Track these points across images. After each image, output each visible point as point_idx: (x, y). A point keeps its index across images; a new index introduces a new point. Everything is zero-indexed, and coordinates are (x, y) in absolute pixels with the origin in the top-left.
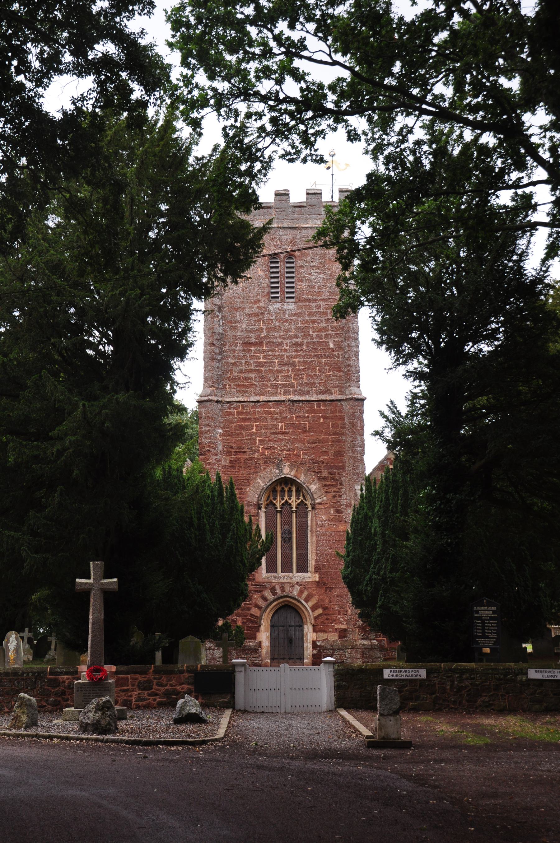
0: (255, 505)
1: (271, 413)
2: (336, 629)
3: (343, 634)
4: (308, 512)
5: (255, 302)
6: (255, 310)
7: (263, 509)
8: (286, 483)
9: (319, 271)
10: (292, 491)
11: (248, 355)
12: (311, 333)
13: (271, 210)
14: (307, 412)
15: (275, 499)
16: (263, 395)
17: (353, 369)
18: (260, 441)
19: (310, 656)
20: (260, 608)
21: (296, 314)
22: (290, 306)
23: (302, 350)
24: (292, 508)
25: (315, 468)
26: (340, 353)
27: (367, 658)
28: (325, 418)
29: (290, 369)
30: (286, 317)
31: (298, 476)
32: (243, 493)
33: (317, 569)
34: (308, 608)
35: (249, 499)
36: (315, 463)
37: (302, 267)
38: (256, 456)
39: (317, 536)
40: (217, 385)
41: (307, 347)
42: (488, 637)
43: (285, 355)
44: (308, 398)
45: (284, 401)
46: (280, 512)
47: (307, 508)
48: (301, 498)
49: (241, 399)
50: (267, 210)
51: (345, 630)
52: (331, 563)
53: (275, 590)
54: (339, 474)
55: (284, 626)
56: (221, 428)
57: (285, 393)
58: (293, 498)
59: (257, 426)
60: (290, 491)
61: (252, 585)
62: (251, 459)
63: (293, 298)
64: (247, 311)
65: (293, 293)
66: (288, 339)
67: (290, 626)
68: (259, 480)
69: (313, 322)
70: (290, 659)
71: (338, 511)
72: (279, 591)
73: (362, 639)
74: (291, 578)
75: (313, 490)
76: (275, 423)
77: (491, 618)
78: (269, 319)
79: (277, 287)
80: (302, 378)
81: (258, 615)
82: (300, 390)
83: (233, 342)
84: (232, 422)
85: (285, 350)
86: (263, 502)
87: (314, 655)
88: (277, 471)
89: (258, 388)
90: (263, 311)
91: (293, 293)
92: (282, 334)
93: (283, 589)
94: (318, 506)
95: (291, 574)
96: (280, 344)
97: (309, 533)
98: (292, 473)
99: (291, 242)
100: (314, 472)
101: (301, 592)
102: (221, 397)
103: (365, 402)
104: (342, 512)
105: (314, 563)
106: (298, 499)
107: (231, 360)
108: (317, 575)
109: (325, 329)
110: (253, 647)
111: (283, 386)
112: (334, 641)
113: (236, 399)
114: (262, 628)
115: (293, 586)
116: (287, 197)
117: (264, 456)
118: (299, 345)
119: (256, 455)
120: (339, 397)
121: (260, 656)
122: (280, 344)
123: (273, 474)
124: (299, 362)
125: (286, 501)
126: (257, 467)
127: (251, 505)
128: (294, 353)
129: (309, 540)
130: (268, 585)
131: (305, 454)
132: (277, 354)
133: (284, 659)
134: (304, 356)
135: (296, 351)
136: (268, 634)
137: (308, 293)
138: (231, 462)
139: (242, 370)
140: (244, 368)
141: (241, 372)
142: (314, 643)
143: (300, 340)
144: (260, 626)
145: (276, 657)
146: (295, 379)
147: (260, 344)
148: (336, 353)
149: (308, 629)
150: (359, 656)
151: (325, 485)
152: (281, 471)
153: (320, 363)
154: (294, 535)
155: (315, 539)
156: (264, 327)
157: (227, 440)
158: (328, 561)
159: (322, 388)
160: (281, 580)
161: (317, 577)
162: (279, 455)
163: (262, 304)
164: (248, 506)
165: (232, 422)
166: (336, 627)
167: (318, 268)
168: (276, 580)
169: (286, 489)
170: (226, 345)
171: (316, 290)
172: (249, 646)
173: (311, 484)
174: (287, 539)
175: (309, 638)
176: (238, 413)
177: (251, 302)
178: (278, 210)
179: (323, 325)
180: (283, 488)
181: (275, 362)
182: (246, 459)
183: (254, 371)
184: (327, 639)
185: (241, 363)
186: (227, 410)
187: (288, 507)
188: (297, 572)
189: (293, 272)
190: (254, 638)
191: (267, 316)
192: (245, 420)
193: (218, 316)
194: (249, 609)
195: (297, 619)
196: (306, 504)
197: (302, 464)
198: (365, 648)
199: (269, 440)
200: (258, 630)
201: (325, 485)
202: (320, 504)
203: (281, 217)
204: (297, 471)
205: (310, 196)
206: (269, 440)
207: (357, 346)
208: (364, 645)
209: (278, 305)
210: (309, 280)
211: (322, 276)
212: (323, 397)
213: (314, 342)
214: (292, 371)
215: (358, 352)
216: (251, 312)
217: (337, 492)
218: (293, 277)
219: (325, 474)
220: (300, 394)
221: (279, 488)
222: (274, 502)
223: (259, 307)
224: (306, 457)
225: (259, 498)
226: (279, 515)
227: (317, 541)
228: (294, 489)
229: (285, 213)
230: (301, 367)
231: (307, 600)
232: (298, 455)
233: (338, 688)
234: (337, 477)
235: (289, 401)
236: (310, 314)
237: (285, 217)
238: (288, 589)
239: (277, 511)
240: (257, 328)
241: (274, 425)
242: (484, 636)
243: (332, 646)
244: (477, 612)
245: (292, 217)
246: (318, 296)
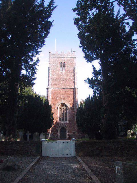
3: (74, 133)
6: (58, 72)
33: (69, 121)
42: (122, 131)
71: (73, 109)
77: (124, 125)
90: (59, 72)
114: (58, 132)
138: (53, 100)
142: (68, 135)
149: (67, 132)
150: (77, 137)
219: (71, 102)
231: (67, 126)
233: (76, 149)
242: (122, 131)
244: (119, 123)
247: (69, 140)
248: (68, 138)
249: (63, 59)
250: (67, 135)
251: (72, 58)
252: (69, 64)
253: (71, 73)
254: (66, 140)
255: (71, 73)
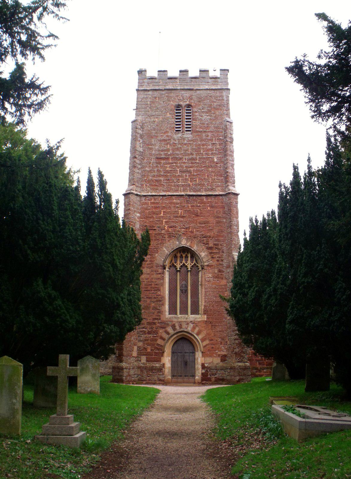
0: (161, 266)
1: (174, 203)
2: (219, 355)
4: (199, 271)
5: (165, 133)
6: (164, 137)
7: (167, 269)
8: (184, 251)
9: (208, 115)
10: (188, 257)
11: (159, 166)
12: (202, 152)
13: (177, 80)
14: (199, 203)
15: (176, 263)
16: (169, 191)
17: (230, 175)
18: (166, 222)
19: (200, 374)
20: (164, 339)
21: (191, 141)
22: (188, 135)
23: (196, 163)
24: (188, 269)
25: (204, 240)
26: (222, 165)
27: (241, 375)
28: (212, 207)
29: (187, 175)
30: (186, 142)
31: (192, 246)
32: (153, 258)
34: (199, 340)
35: (157, 262)
36: (204, 237)
37: (196, 112)
38: (163, 232)
39: (205, 289)
40: (137, 184)
41: (199, 160)
43: (184, 165)
44: (199, 193)
45: (183, 195)
46: (179, 271)
47: (199, 269)
48: (194, 262)
49: (154, 194)
50: (174, 80)
51: (225, 356)
52: (215, 307)
53: (175, 327)
54: (221, 245)
55: (181, 353)
56: (139, 213)
57: (184, 191)
58: (189, 262)
59: (164, 212)
60: (186, 257)
61: (159, 323)
62: (160, 234)
63: (190, 131)
64: (159, 138)
65: (190, 128)
66: (186, 155)
67: (185, 353)
68: (164, 249)
69: (203, 145)
70: (185, 376)
72: (177, 327)
73: (238, 362)
74: (187, 318)
75: (202, 256)
76: (177, 210)
78: (174, 143)
79: (180, 125)
80: (196, 181)
81: (163, 345)
82: (194, 188)
83: (149, 158)
84: (147, 209)
85: (184, 163)
86: (167, 263)
87: (202, 374)
88: (177, 243)
89: (165, 187)
91: (190, 128)
92: (182, 152)
93: (181, 326)
94: (205, 268)
95: (186, 316)
96: (181, 159)
97: (200, 286)
98: (188, 244)
99: (189, 98)
100: (203, 243)
101: (194, 328)
102: (140, 192)
103: (239, 196)
104: (223, 272)
105: (203, 308)
106: (193, 263)
107: (147, 169)
108: (205, 316)
109: (212, 150)
110: (158, 368)
111: (183, 186)
112: (217, 364)
113: (150, 194)
114: (165, 354)
115: (188, 324)
116: (187, 73)
117: (168, 233)
118: (194, 159)
119: (163, 232)
120: (221, 193)
121: (163, 374)
122: (181, 159)
123: (176, 244)
124: (194, 170)
125: (184, 264)
126: (164, 240)
127: (158, 266)
128: (190, 165)
129: (200, 291)
130: (170, 323)
131: (198, 231)
132: (179, 165)
133: (181, 376)
134: (197, 167)
135: (192, 163)
136: (170, 358)
137: (201, 128)
139: (154, 175)
140: (156, 174)
141: (154, 176)
143: (194, 156)
144: (164, 352)
145: (175, 375)
146: (191, 181)
147: (168, 159)
148: (219, 165)
150: (236, 374)
151: (211, 253)
152: (180, 243)
153: (208, 171)
154: (189, 288)
155: (204, 290)
156: (170, 148)
157: (143, 221)
158: (213, 306)
159: (209, 187)
160: (180, 320)
161: (205, 318)
162: (179, 231)
163: (169, 134)
164: (157, 267)
165: (147, 209)
166: (219, 353)
167: (207, 113)
168: (176, 320)
169: (184, 256)
170: (144, 159)
171: (206, 126)
172: (156, 367)
173: (201, 252)
174: (184, 291)
175: (199, 361)
176: (151, 203)
177: (162, 133)
178: (181, 80)
179: (210, 147)
180: (181, 255)
181: (177, 170)
182: (156, 234)
183: (163, 176)
184: (212, 362)
185: (154, 171)
186: (144, 201)
187: (185, 269)
188: (191, 314)
189: (190, 116)
190: (159, 360)
191: (172, 141)
192: (156, 208)
193: (139, 141)
194: (156, 340)
195: (191, 348)
196: (197, 266)
197: (195, 238)
198: (241, 369)
199: (173, 222)
200: (162, 356)
201: (211, 253)
202: (208, 266)
203: (183, 84)
204: (191, 242)
205: (202, 73)
206: (173, 222)
207: (233, 161)
208: (239, 366)
209: (180, 135)
210: (201, 120)
211: (209, 117)
212: (210, 193)
213: (204, 158)
214: (189, 176)
215: (234, 165)
216: (162, 139)
217: (220, 257)
218: (190, 119)
220: (194, 191)
221: (179, 255)
222: (175, 264)
223: (167, 136)
224: (198, 233)
225: (164, 261)
226: (178, 273)
227: (205, 292)
228: (189, 255)
229: (186, 81)
230: (195, 174)
232: (192, 232)
234: (220, 247)
235: (186, 195)
236: (202, 140)
237: (186, 84)
238: (184, 326)
239: (177, 271)
240: (165, 149)
241: (175, 211)
243: (216, 367)
245: (190, 84)
246: (207, 129)
247: (204, 384)
248: (203, 380)
249: (187, 94)
250: (199, 366)
251: (218, 94)
252: (205, 110)
253: (212, 140)
254: (195, 383)
255: (212, 140)
